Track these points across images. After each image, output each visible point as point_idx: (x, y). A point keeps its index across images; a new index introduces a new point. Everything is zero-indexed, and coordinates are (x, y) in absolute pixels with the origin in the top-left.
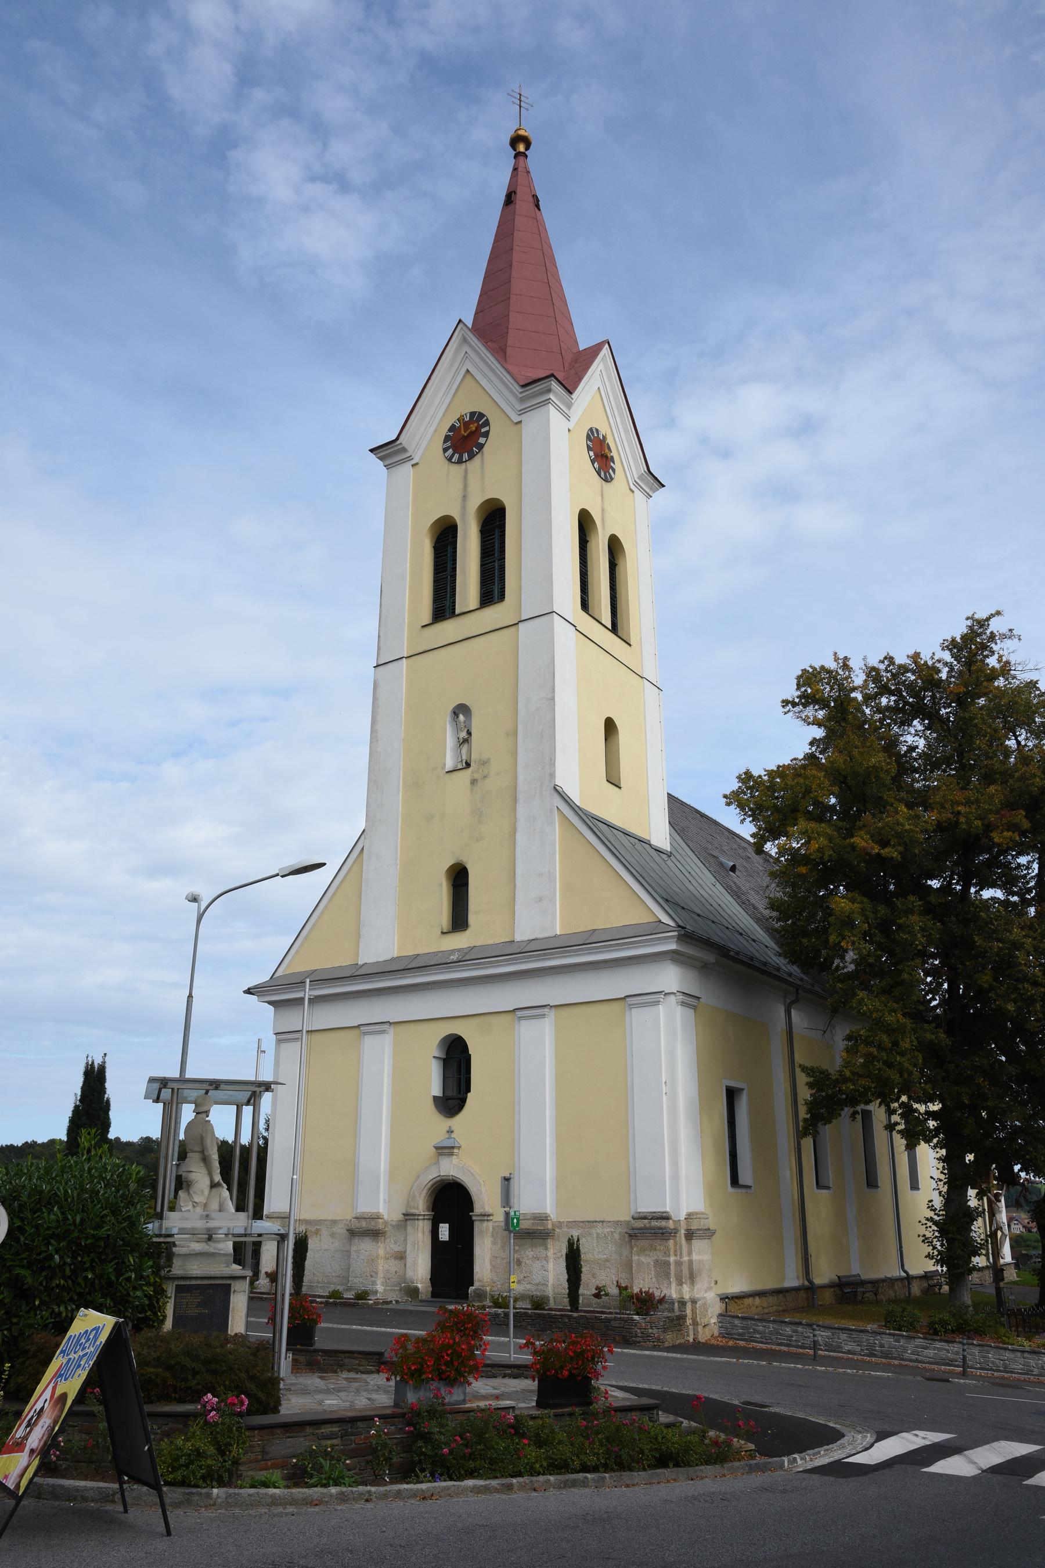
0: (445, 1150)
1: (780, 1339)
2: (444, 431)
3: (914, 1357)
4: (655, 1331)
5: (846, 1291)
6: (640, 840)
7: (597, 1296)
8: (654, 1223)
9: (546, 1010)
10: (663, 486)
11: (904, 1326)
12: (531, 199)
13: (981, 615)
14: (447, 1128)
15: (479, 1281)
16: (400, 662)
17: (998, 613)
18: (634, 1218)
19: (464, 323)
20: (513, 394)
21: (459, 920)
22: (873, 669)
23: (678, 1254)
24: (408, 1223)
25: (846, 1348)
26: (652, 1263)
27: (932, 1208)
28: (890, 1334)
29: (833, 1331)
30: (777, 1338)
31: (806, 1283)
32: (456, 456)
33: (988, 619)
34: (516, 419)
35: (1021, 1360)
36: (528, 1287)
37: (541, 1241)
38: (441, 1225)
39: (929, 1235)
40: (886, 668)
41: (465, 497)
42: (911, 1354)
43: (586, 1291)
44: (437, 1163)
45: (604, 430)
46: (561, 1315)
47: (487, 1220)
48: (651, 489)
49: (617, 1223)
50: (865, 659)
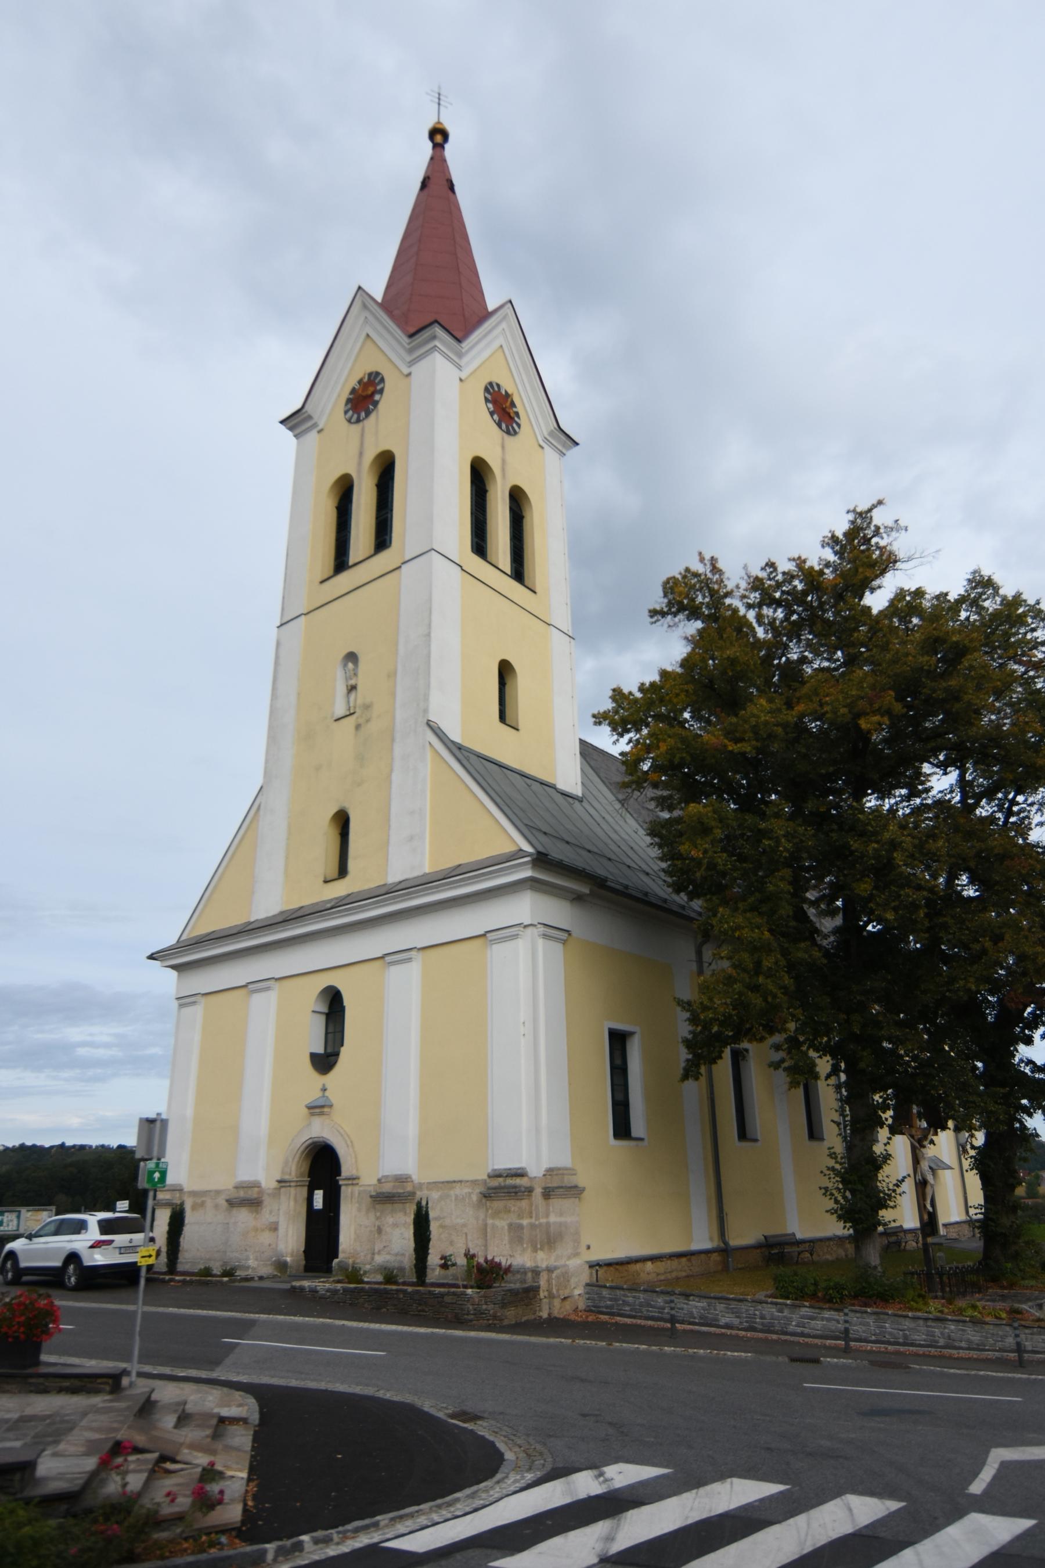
0: (318, 1109)
1: (651, 1312)
2: (346, 394)
3: (799, 1330)
4: (491, 1306)
5: (773, 1252)
6: (541, 783)
7: (445, 1266)
8: (510, 1181)
9: (413, 953)
10: (577, 444)
11: (791, 1293)
12: (445, 183)
13: (862, 507)
14: (321, 1087)
15: (344, 1252)
16: (299, 619)
17: (880, 503)
18: (489, 1176)
19: (364, 291)
20: (403, 346)
21: (343, 871)
22: (757, 578)
23: (534, 1215)
24: (283, 1190)
25: (723, 1321)
26: (506, 1227)
27: (832, 1155)
28: (772, 1303)
29: (709, 1300)
30: (648, 1311)
31: (722, 1245)
32: (355, 416)
33: (870, 510)
34: (406, 371)
35: (923, 1329)
36: (388, 1257)
37: (401, 1205)
38: (316, 1192)
39: (830, 1185)
40: (769, 575)
41: (361, 454)
42: (796, 1326)
43: (434, 1259)
44: (309, 1125)
45: (507, 386)
46: (397, 1291)
47: (353, 1184)
48: (564, 446)
49: (474, 1182)
50: (745, 567)
